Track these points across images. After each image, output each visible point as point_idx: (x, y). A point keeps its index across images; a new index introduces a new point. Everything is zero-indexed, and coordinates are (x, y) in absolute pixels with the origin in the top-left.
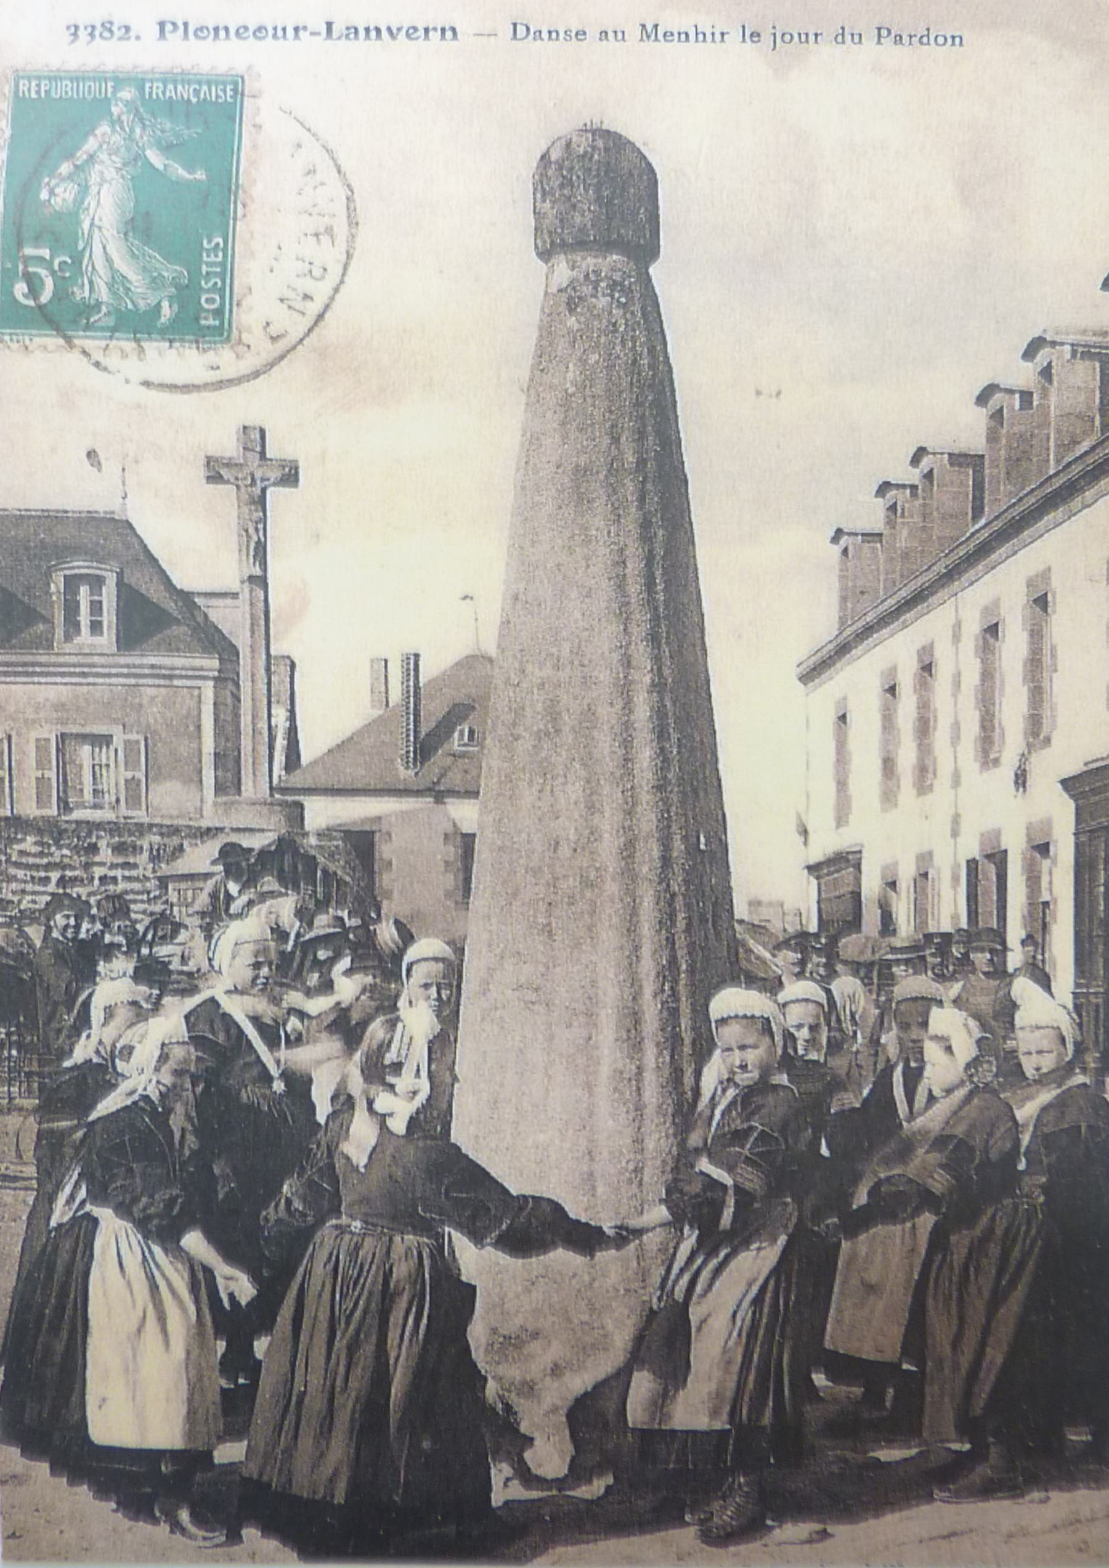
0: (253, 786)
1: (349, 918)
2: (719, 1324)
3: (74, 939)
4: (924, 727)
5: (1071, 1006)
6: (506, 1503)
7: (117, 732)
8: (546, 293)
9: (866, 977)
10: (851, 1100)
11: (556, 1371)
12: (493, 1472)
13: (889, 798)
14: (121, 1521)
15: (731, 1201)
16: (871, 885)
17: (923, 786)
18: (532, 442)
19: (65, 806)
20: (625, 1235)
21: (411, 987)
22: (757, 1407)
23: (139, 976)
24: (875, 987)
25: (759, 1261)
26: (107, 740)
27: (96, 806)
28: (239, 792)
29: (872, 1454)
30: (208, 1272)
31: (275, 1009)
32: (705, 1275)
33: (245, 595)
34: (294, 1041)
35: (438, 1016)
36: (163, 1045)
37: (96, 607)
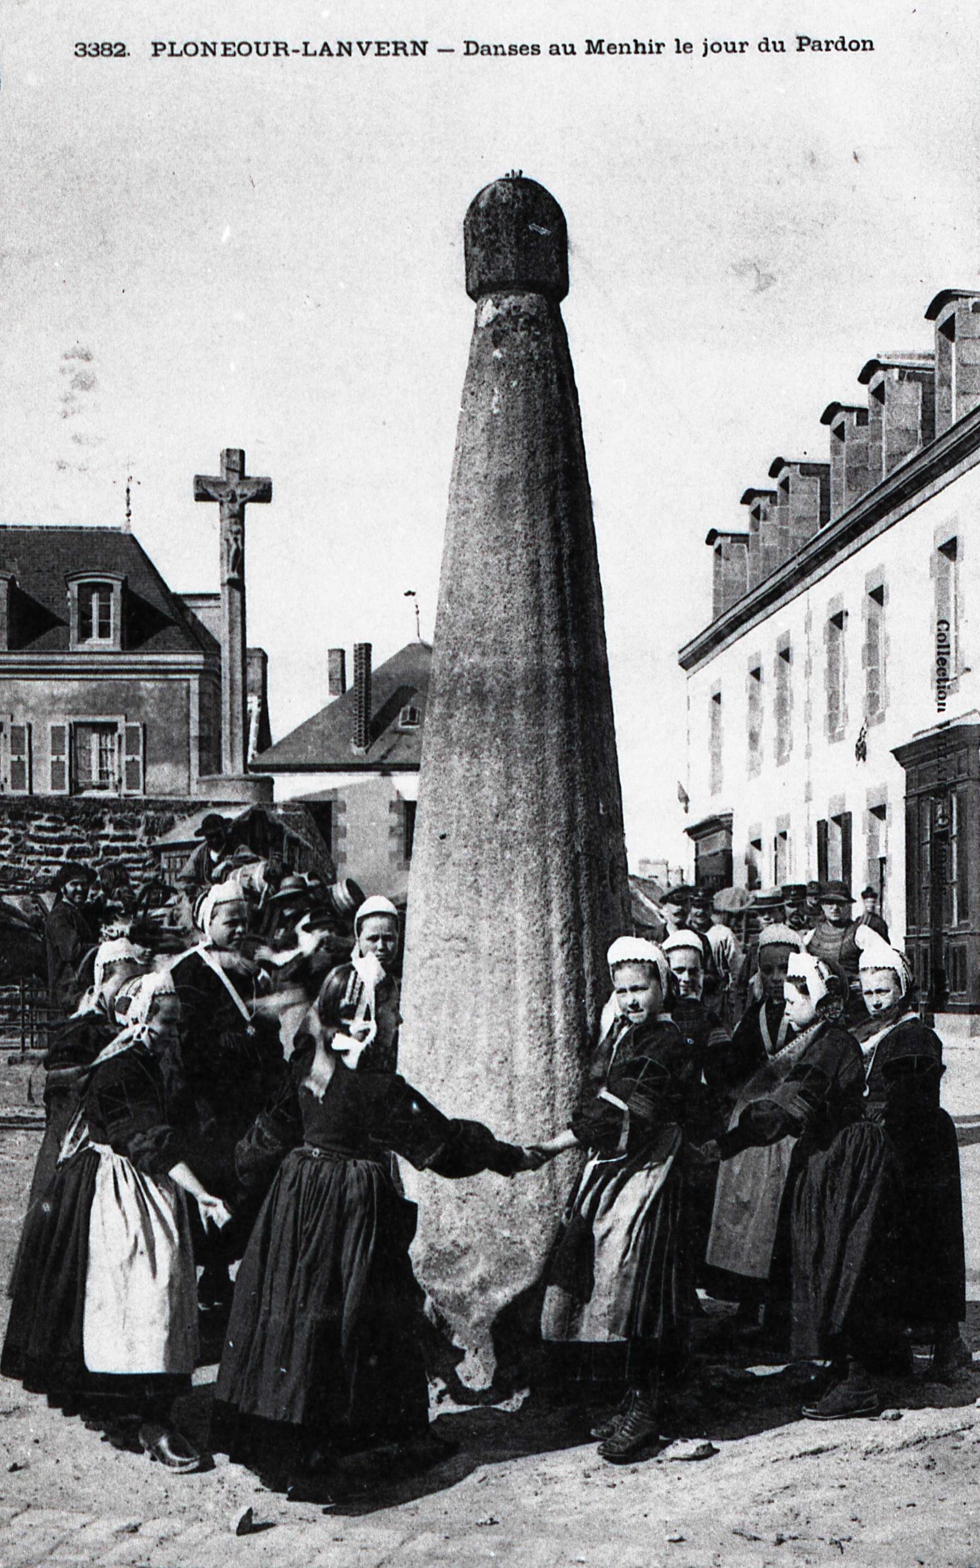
0: (232, 766)
1: (310, 879)
2: (617, 1240)
3: (81, 903)
4: (782, 705)
5: (903, 950)
6: (440, 1417)
7: (120, 720)
8: (476, 329)
9: (736, 924)
10: (724, 1035)
11: (483, 1286)
12: (430, 1386)
13: (754, 767)
14: (108, 1452)
15: (626, 1126)
16: (740, 848)
17: (781, 759)
18: (463, 454)
19: (76, 788)
20: (542, 1157)
21: (362, 942)
22: (649, 1325)
23: (133, 938)
24: (743, 934)
25: (651, 1179)
26: (112, 727)
27: (103, 787)
28: (219, 770)
29: (749, 1369)
30: (191, 1200)
31: (247, 962)
32: (606, 1193)
33: (225, 597)
34: (266, 990)
35: (383, 965)
36: (154, 997)
37: (105, 612)
